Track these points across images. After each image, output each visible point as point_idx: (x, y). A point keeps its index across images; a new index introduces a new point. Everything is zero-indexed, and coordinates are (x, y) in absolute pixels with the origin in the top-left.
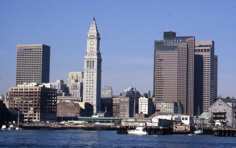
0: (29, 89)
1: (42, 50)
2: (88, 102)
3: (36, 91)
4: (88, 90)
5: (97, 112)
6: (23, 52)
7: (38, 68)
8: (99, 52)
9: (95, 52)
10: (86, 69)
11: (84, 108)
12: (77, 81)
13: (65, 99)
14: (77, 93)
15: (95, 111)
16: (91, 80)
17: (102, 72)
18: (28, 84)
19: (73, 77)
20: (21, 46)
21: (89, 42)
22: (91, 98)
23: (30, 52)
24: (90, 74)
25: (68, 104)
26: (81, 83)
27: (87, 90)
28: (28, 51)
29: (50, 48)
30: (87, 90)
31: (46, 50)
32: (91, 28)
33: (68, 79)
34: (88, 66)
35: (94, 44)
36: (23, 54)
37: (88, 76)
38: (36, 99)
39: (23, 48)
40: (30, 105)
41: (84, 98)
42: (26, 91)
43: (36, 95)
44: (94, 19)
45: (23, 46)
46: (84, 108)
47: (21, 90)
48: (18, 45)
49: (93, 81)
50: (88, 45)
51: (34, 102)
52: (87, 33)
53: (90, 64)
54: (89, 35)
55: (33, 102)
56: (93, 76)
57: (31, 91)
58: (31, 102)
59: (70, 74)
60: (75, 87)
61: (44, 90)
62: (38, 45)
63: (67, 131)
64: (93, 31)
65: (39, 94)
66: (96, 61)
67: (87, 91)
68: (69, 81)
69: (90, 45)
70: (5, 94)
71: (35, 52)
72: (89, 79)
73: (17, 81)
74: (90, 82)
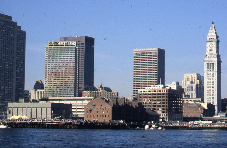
0: (157, 91)
1: (157, 54)
2: (209, 102)
3: (164, 92)
4: (209, 91)
5: (218, 112)
6: (139, 56)
7: (140, 71)
8: (219, 54)
9: (215, 55)
10: (206, 71)
11: (207, 108)
12: (192, 82)
13: (186, 100)
14: (193, 94)
15: (216, 111)
16: (212, 82)
17: (221, 73)
18: (155, 86)
19: (188, 79)
20: (137, 50)
21: (209, 44)
22: (212, 99)
23: (146, 56)
24: (210, 75)
25: (191, 104)
26: (196, 84)
27: (208, 91)
28: (144, 55)
29: (164, 52)
30: (208, 91)
31: (161, 53)
32: (210, 31)
33: (183, 81)
34: (208, 68)
35: (214, 47)
36: (139, 58)
37: (208, 78)
38: (164, 100)
39: (140, 52)
40: (158, 106)
41: (205, 99)
42: (154, 93)
43: (163, 97)
44: (213, 23)
45: (140, 50)
46: (207, 108)
47: (154, 92)
48: (135, 50)
49: (213, 82)
50: (207, 47)
51: (162, 103)
52: (206, 36)
53: (210, 65)
54: (208, 39)
55: (161, 104)
56: (213, 78)
57: (159, 93)
58: (159, 104)
59: (185, 76)
60: (191, 88)
61: (171, 92)
62: (154, 49)
63: (205, 131)
64: (212, 34)
65: (167, 96)
66: (216, 63)
67: (208, 93)
68: (184, 82)
69: (210, 48)
70: (130, 96)
71: (151, 55)
72: (209, 81)
73: (134, 83)
74: (210, 83)
